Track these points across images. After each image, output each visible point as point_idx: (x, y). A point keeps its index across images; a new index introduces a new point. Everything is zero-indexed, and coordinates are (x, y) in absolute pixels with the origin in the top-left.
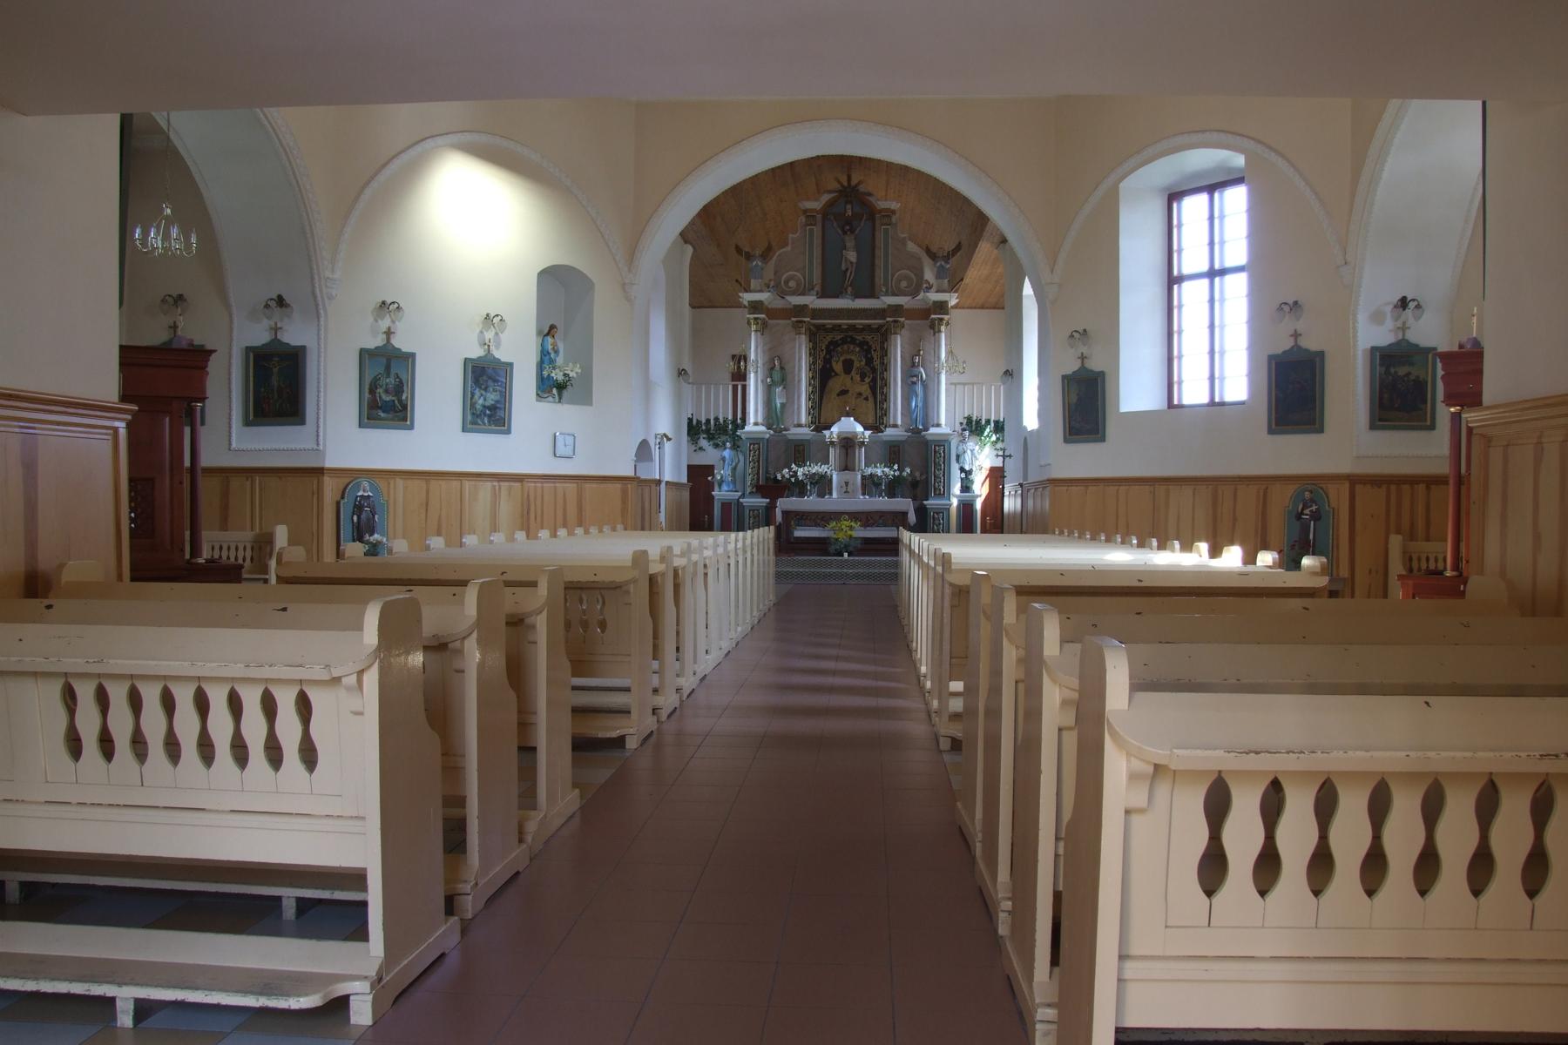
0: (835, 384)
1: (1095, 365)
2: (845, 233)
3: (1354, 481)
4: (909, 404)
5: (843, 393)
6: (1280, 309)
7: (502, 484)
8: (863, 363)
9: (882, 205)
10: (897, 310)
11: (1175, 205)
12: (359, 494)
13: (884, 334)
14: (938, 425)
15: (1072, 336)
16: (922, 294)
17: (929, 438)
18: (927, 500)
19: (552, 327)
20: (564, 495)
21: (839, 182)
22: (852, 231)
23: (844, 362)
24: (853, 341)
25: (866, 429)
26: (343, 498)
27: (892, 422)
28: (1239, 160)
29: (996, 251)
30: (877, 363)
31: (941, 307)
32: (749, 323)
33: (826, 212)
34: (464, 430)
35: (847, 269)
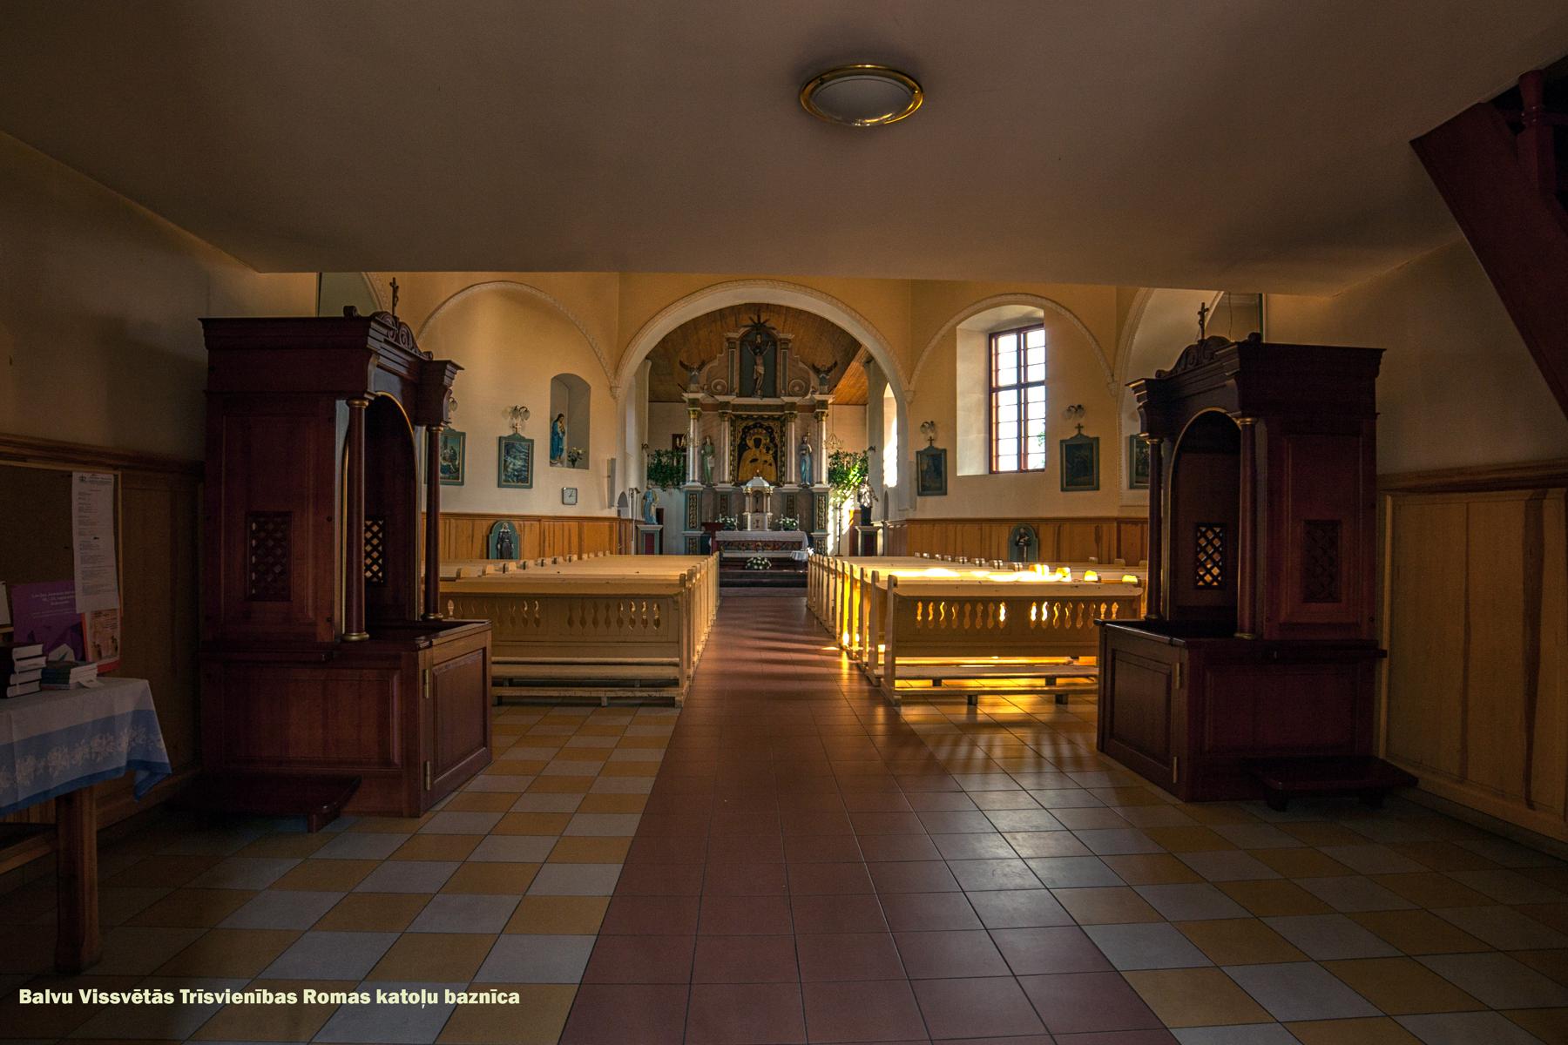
0: (748, 455)
1: (939, 445)
2: (756, 354)
3: (1120, 521)
4: (801, 468)
5: (754, 460)
6: (1069, 410)
7: (526, 523)
8: (768, 441)
9: (782, 336)
10: (793, 406)
11: (993, 341)
12: (502, 530)
13: (783, 422)
14: (821, 482)
15: (923, 426)
16: (810, 395)
17: (814, 491)
18: (813, 532)
19: (560, 416)
20: (569, 530)
21: (752, 320)
22: (761, 353)
23: (755, 440)
24: (761, 426)
25: (771, 484)
26: (491, 533)
27: (788, 480)
28: (1041, 313)
29: (862, 368)
30: (777, 440)
31: (824, 404)
32: (689, 414)
33: (743, 339)
34: (499, 485)
35: (757, 379)
